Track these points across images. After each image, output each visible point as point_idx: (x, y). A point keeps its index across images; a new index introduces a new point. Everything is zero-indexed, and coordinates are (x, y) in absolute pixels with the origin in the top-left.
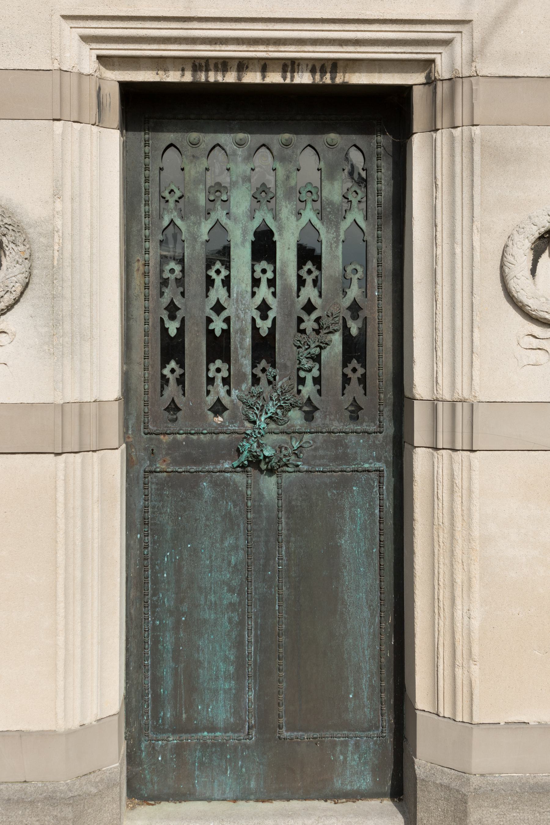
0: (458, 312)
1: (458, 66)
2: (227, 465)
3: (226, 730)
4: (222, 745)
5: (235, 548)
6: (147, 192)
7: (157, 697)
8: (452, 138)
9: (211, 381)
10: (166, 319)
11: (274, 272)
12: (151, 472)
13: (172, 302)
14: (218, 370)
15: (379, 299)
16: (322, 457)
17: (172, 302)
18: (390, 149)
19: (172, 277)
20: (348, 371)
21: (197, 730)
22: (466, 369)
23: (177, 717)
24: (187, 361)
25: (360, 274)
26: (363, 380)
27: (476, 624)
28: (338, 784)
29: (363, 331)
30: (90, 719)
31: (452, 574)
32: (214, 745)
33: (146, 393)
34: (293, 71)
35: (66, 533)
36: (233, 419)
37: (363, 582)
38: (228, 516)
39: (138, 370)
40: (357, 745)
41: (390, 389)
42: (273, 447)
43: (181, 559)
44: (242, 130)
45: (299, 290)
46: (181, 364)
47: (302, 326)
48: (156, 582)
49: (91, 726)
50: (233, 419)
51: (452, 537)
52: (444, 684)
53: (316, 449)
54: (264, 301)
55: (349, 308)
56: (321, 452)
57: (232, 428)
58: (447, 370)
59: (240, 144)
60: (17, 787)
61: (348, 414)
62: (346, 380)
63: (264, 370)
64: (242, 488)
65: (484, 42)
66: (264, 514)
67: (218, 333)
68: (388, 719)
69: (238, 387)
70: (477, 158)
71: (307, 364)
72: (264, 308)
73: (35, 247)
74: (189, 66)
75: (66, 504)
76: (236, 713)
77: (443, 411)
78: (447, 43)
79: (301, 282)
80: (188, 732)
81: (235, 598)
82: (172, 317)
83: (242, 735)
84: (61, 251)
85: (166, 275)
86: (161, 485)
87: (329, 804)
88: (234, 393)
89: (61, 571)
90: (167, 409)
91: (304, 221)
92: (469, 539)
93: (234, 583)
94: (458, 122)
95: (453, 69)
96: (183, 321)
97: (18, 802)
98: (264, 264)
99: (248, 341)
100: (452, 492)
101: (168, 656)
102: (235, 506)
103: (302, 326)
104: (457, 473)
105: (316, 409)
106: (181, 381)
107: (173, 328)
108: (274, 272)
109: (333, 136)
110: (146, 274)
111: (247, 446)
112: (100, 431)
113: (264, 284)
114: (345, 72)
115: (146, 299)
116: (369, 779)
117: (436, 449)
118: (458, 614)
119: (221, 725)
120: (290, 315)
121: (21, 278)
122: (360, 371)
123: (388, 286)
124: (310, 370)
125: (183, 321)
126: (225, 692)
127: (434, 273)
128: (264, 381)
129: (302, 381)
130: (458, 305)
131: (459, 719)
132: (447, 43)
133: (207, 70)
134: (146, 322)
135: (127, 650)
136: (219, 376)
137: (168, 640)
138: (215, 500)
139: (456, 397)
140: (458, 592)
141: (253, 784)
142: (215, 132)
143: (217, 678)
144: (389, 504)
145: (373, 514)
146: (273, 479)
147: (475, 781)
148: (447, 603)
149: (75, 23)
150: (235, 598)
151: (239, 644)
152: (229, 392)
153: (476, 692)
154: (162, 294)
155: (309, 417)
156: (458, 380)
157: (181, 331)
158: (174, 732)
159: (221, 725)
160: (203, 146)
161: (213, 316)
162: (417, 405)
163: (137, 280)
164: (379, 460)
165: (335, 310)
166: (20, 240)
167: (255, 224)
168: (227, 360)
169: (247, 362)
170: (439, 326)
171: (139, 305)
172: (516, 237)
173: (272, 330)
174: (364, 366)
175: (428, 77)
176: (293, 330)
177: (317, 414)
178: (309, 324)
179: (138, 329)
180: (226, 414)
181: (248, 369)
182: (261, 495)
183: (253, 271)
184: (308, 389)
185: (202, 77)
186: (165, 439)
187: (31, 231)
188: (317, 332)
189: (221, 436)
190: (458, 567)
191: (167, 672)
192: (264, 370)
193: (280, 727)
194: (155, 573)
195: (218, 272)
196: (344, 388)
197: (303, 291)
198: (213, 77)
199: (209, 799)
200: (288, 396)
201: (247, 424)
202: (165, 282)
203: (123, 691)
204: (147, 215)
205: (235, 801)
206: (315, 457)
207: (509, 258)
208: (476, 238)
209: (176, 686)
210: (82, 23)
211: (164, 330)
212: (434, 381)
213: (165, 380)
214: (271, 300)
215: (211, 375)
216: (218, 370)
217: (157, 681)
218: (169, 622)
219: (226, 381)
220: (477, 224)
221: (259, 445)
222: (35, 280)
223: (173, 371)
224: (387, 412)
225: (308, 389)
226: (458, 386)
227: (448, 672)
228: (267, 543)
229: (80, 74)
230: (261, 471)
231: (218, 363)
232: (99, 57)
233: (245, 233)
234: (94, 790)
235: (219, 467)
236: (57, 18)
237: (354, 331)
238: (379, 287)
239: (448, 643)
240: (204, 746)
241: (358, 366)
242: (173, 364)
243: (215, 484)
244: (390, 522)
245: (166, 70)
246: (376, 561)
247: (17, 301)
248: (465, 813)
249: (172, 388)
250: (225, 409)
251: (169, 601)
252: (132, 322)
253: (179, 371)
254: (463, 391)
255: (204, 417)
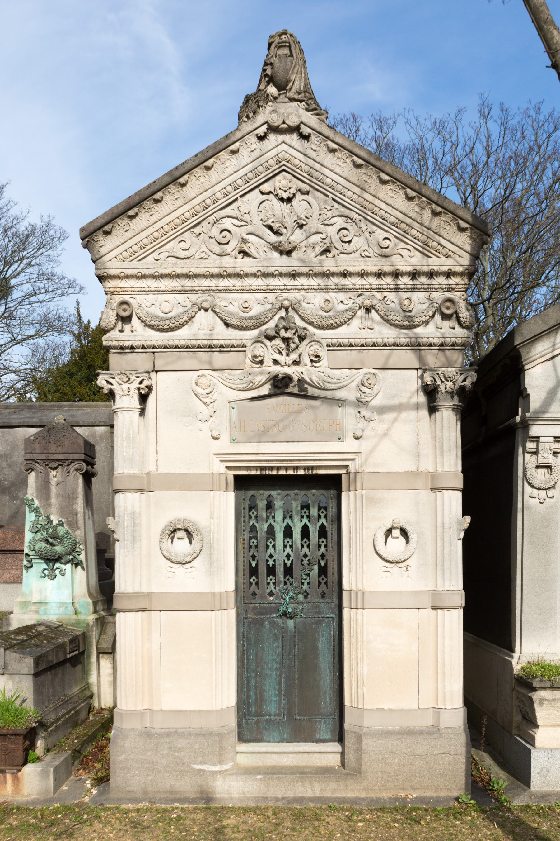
0: (358, 558)
1: (357, 468)
2: (274, 616)
3: (275, 716)
4: (274, 721)
5: (278, 647)
6: (244, 513)
7: (249, 703)
8: (355, 494)
9: (268, 584)
10: (251, 560)
11: (292, 542)
12: (246, 618)
13: (253, 554)
14: (271, 580)
15: (332, 552)
16: (310, 612)
17: (253, 554)
18: (336, 495)
19: (254, 545)
20: (321, 580)
21: (264, 715)
22: (361, 578)
23: (256, 711)
24: (259, 577)
25: (325, 543)
26: (326, 583)
27: (365, 672)
28: (318, 736)
29: (326, 564)
30: (224, 707)
31: (357, 654)
32: (270, 721)
33: (244, 588)
34: (297, 470)
35: (216, 639)
36: (277, 598)
37: (327, 659)
38: (275, 635)
39: (241, 580)
40: (325, 722)
41: (337, 586)
42: (292, 609)
43: (258, 651)
44: (279, 489)
45: (301, 549)
46: (257, 577)
47: (303, 563)
48: (248, 660)
49: (225, 709)
50: (277, 598)
51: (357, 641)
52: (355, 695)
53: (308, 609)
54: (288, 553)
55: (321, 556)
56: (310, 610)
57: (277, 601)
58: (354, 579)
59: (279, 494)
60: (199, 729)
61: (320, 596)
62: (320, 583)
63: (288, 580)
64: (281, 624)
65: (366, 460)
66: (289, 634)
67: (271, 565)
68: (337, 712)
69: (279, 586)
70: (364, 502)
71: (305, 577)
72: (288, 556)
73: (204, 536)
74: (259, 469)
75: (215, 628)
76: (279, 709)
77: (353, 594)
78: (353, 460)
79: (302, 546)
80: (260, 716)
81: (278, 666)
82: (254, 560)
83: (281, 718)
84: (213, 538)
85: (251, 544)
86: (250, 623)
87: (314, 744)
88: (277, 588)
89: (214, 653)
90: (252, 594)
91: (303, 523)
92: (363, 642)
93: (278, 660)
94: (357, 488)
95: (355, 469)
96: (258, 561)
97: (199, 735)
98: (288, 539)
99: (282, 568)
100: (357, 624)
101: (253, 687)
102: (278, 631)
103: (303, 563)
104: (358, 617)
105: (308, 594)
106: (257, 584)
107: (254, 564)
108: (292, 542)
109: (314, 491)
110: (243, 544)
111: (282, 608)
112: (227, 602)
113: (288, 547)
114: (316, 470)
115: (244, 553)
116: (330, 735)
117: (351, 608)
118: (359, 669)
119: (273, 714)
120: (298, 558)
121: (199, 547)
122: (325, 580)
123: (335, 547)
124: (306, 579)
125: (258, 561)
126: (275, 701)
127: (350, 543)
128: (288, 584)
129: (303, 583)
130: (358, 555)
131: (359, 707)
132: (353, 460)
133: (266, 470)
134: (244, 562)
135: (238, 685)
136: (271, 582)
137: (253, 682)
138: (270, 629)
139: (358, 589)
140: (359, 661)
141: (285, 736)
142: (269, 490)
143: (271, 696)
144: (336, 630)
145: (330, 634)
146: (292, 621)
147: (365, 730)
148: (355, 665)
149: (218, 456)
150: (278, 666)
151: (280, 683)
152: (275, 588)
153: (365, 697)
154: (250, 551)
155: (306, 597)
156: (358, 583)
157: (257, 565)
158: (255, 716)
159: (273, 714)
160: (265, 495)
161: (269, 559)
162: (344, 592)
163: (240, 546)
164: (332, 613)
165: (315, 556)
166: (199, 534)
167: (285, 524)
168: (274, 575)
169: (282, 577)
170: (352, 563)
171: (241, 555)
172: (378, 531)
173: (291, 564)
174: (326, 578)
175: (347, 471)
176: (299, 564)
177: (309, 596)
178: (305, 562)
179: (241, 564)
180: (274, 596)
181: (282, 579)
182: (288, 627)
183: (284, 542)
184: (305, 587)
185: (264, 473)
186: (251, 606)
187: (202, 530)
188: (309, 565)
189: (272, 605)
190: (359, 652)
191: (252, 693)
192: (288, 580)
193: (296, 715)
194: (248, 656)
195: (271, 543)
196: (319, 586)
197: (303, 549)
198: (268, 472)
199: (269, 742)
200: (297, 589)
201: (282, 600)
202: (251, 547)
203: (236, 701)
204: (244, 522)
205: (279, 742)
206: (308, 612)
207: (376, 538)
208: (364, 531)
209: (256, 699)
210: (220, 456)
211: (251, 565)
212: (350, 584)
213: (251, 583)
214: (291, 553)
215: (268, 581)
216: (271, 580)
217: (249, 697)
218: (253, 674)
219: (274, 584)
220: (364, 526)
221: (286, 608)
222: (204, 548)
223: (254, 580)
224: (336, 595)
225: (305, 587)
226: (358, 585)
227: (356, 691)
228: (290, 645)
229: (220, 474)
230: (288, 618)
231: (271, 577)
232: (226, 467)
233: (281, 527)
234: (226, 732)
235: (271, 616)
236: (211, 454)
237: (323, 564)
238: (332, 547)
239: (356, 680)
240: (267, 721)
241: (324, 578)
242: (254, 577)
243: (270, 623)
244: (337, 637)
245: (250, 470)
246: (332, 652)
247: (197, 556)
248: (361, 741)
249: (254, 586)
250: (274, 594)
251: (253, 667)
252: (238, 562)
253: (256, 580)
254: (360, 587)
255: (265, 597)
